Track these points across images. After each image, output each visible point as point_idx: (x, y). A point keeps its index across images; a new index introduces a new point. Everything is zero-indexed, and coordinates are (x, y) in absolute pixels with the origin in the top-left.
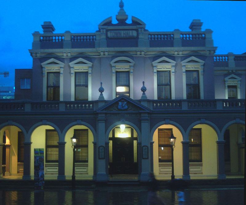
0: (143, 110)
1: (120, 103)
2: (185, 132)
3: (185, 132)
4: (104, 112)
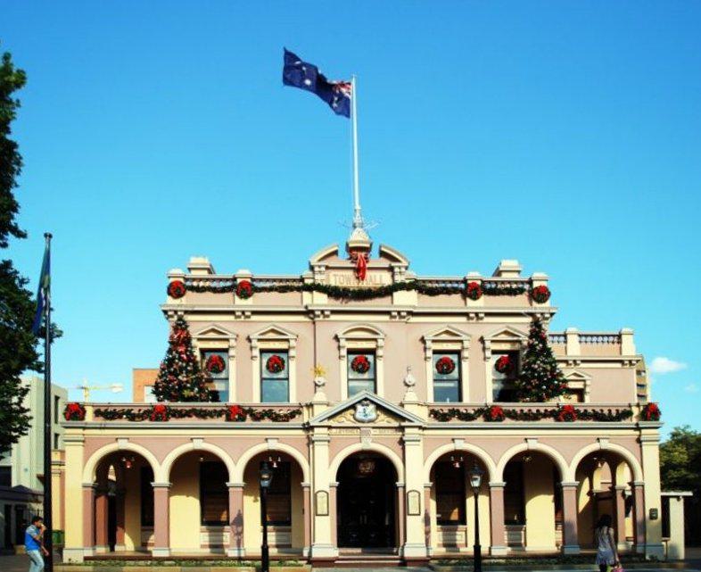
0: (411, 421)
1: (360, 408)
2: (496, 465)
3: (496, 465)
4: (326, 423)
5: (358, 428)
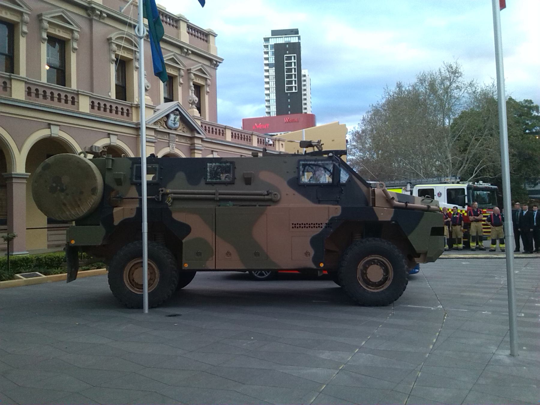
3: (20, 151)
5: (169, 133)
